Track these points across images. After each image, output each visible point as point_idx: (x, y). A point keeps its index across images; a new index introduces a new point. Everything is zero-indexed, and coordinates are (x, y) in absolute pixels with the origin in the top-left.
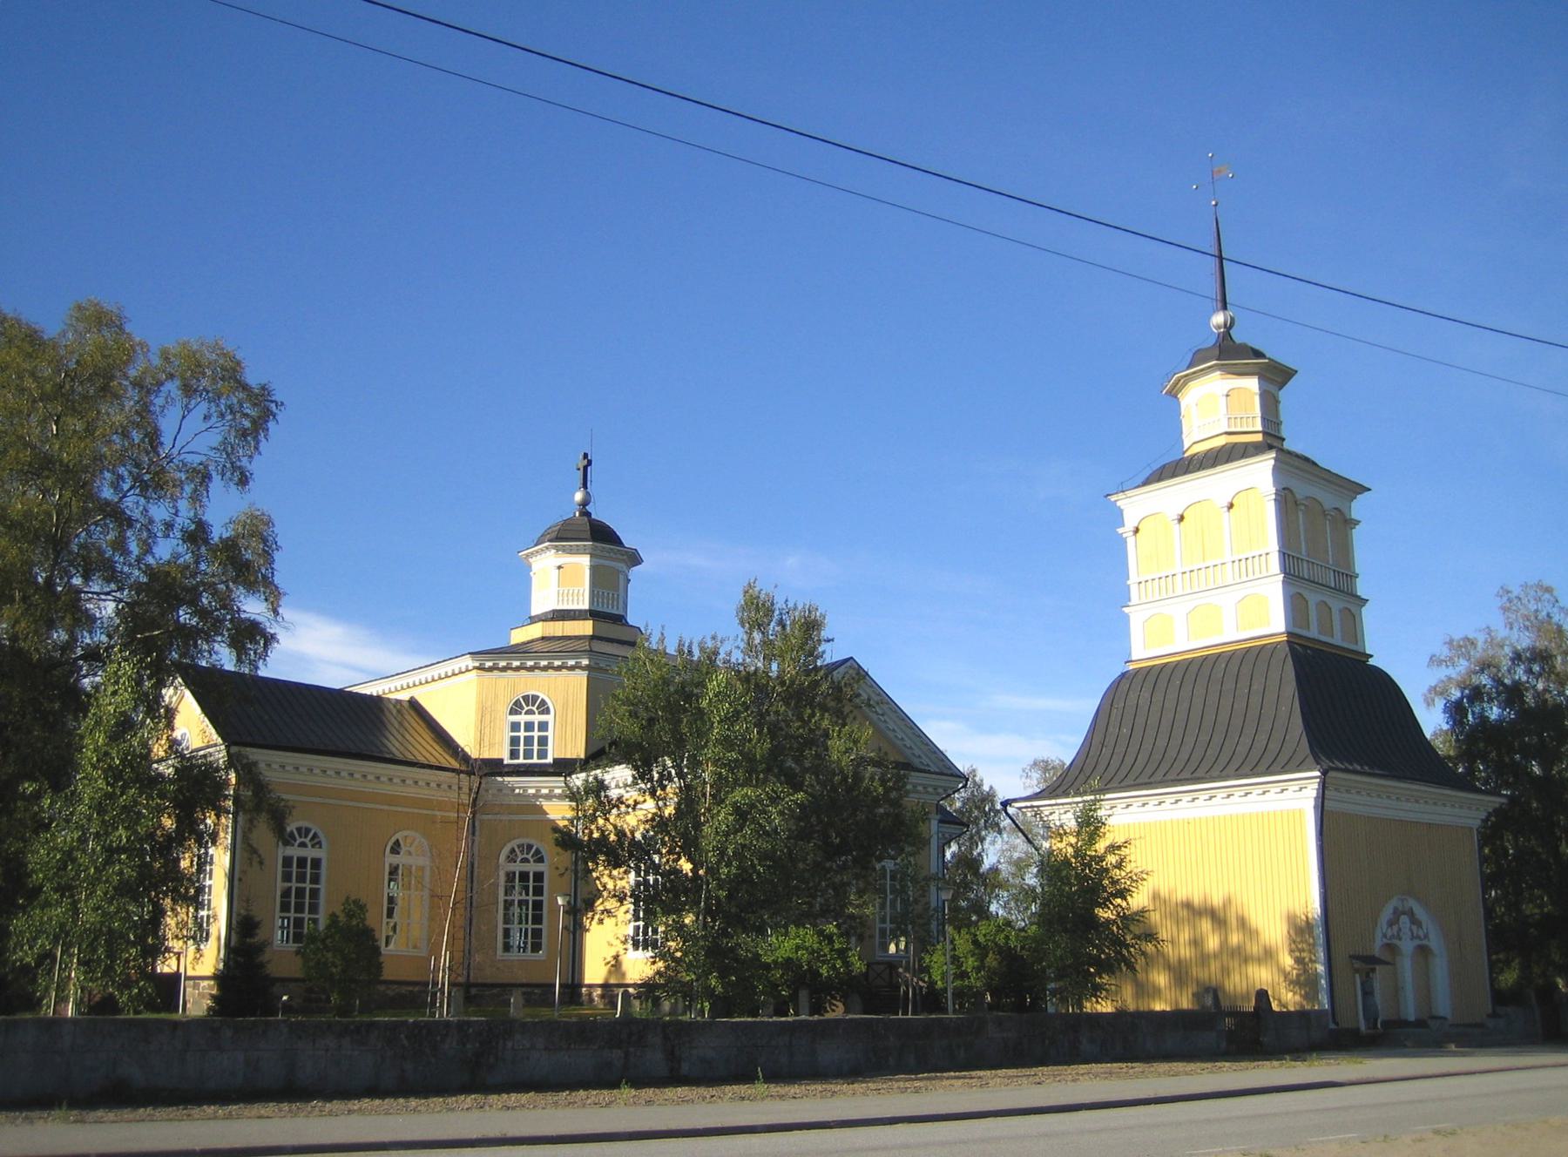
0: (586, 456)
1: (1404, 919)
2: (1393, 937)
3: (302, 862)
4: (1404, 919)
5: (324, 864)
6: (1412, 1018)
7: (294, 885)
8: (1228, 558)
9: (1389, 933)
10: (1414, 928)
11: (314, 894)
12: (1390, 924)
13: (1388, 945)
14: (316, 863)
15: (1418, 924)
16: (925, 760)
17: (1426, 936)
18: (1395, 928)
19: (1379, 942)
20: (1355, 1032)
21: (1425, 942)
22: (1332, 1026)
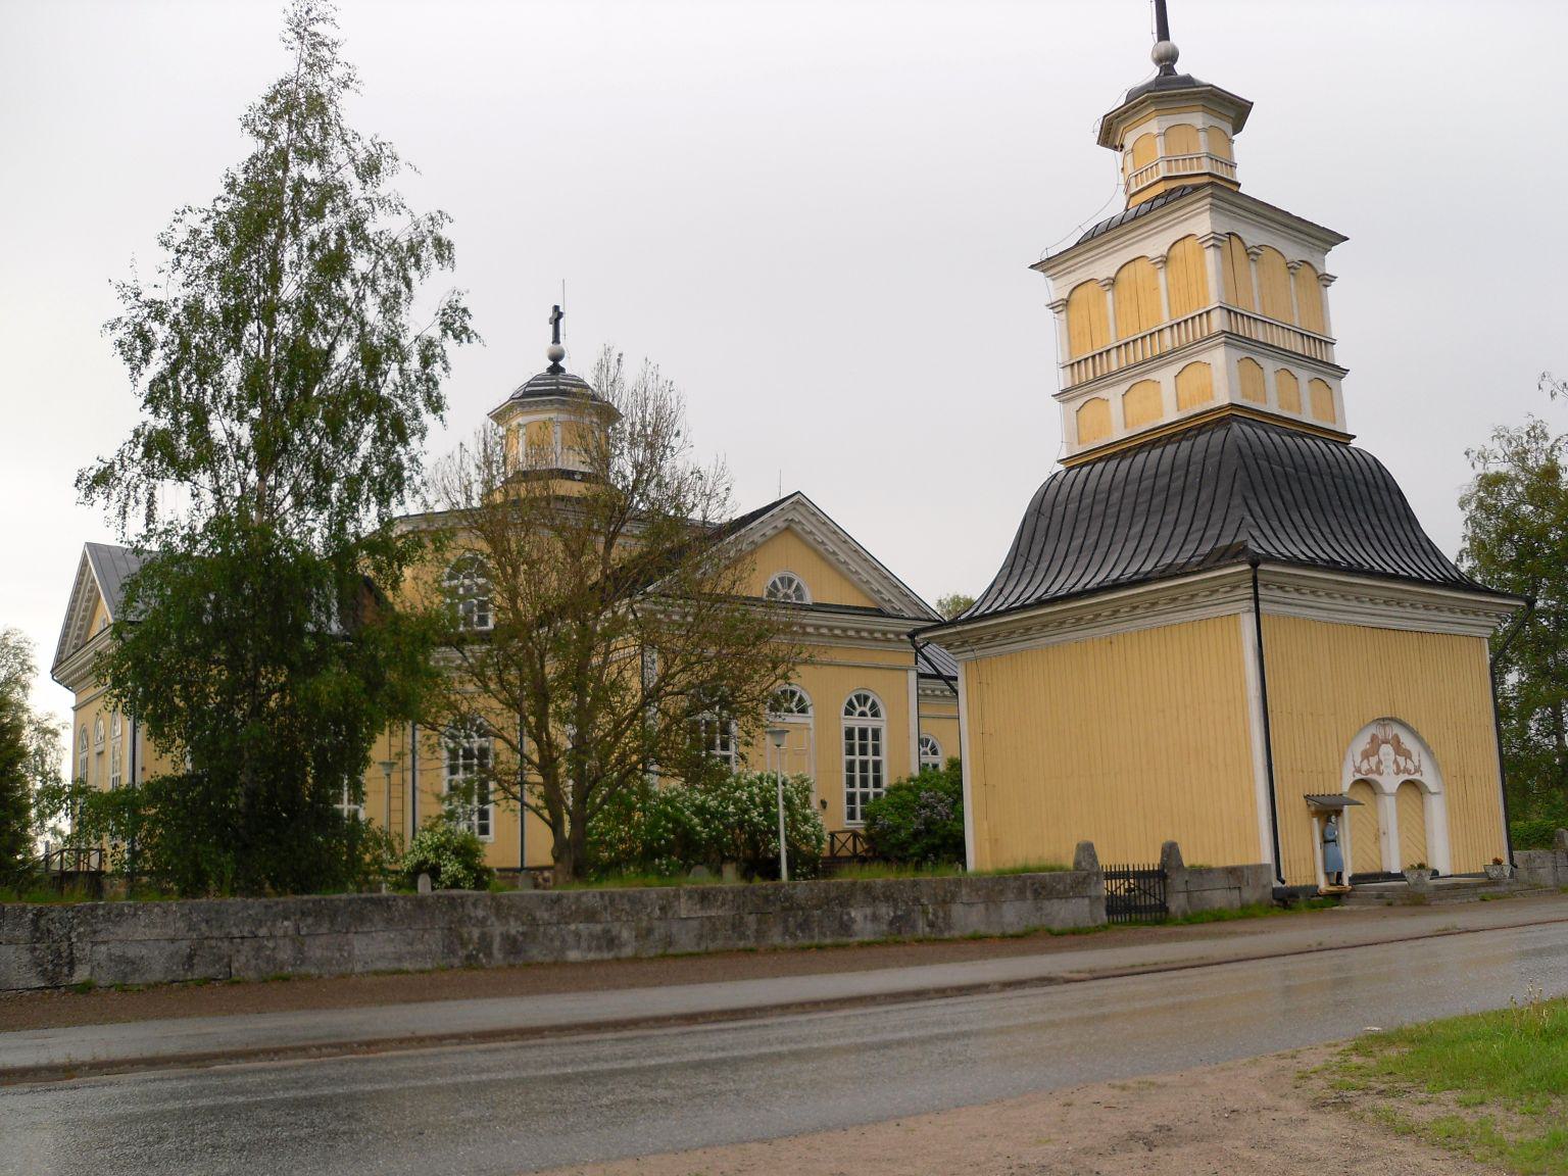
0: (556, 308)
1: (1387, 750)
2: (1370, 771)
3: (863, 733)
4: (1387, 750)
5: (884, 735)
6: (1396, 869)
7: (857, 758)
8: (1166, 321)
9: (1365, 767)
10: (1401, 760)
11: (877, 766)
12: (1366, 755)
13: (1407, 783)
14: (876, 734)
15: (1407, 755)
16: (898, 605)
17: (1418, 770)
18: (1373, 760)
19: (1348, 779)
20: (1311, 891)
21: (1416, 777)
22: (1277, 884)
